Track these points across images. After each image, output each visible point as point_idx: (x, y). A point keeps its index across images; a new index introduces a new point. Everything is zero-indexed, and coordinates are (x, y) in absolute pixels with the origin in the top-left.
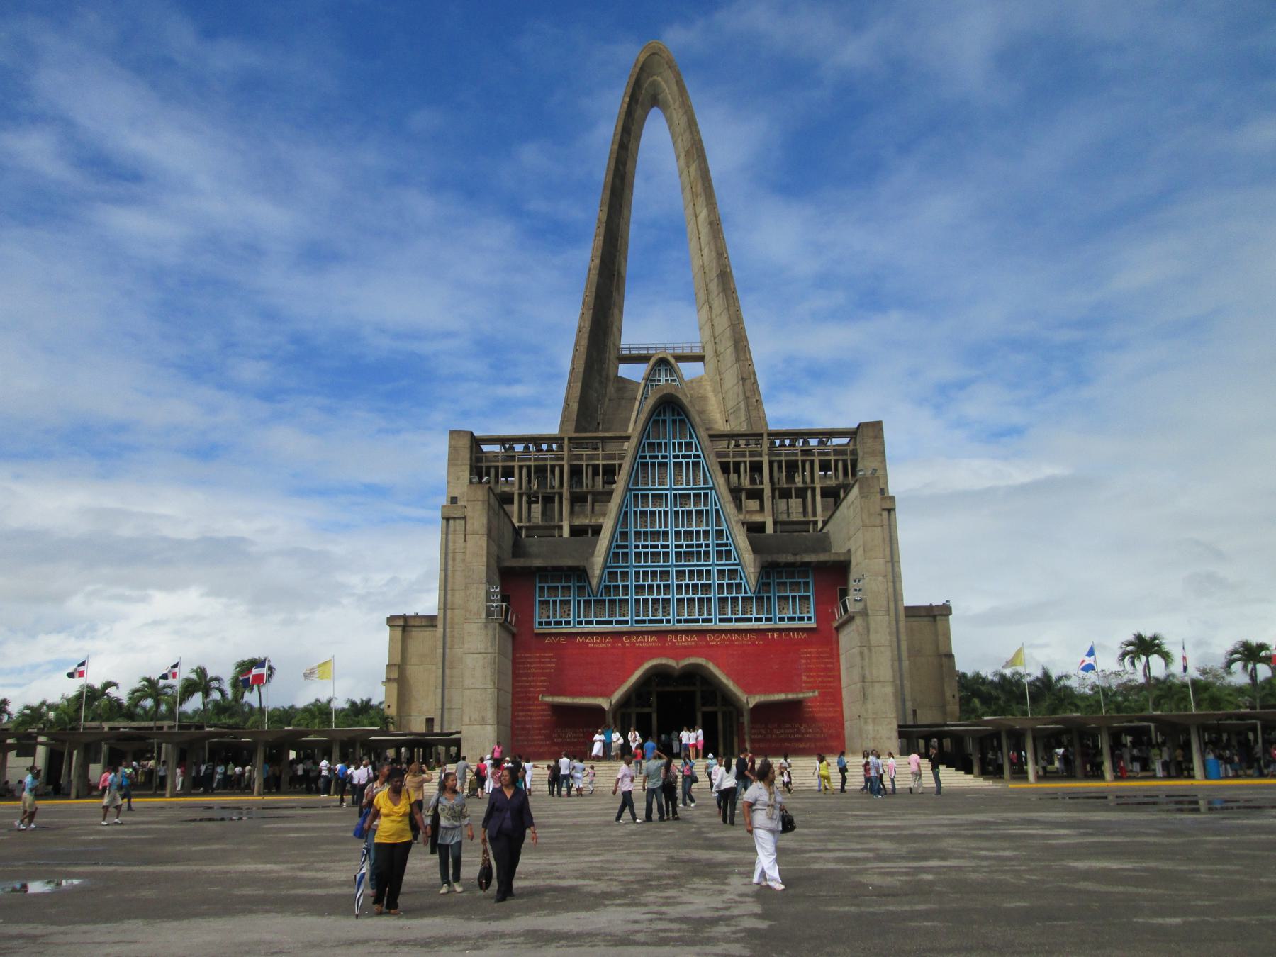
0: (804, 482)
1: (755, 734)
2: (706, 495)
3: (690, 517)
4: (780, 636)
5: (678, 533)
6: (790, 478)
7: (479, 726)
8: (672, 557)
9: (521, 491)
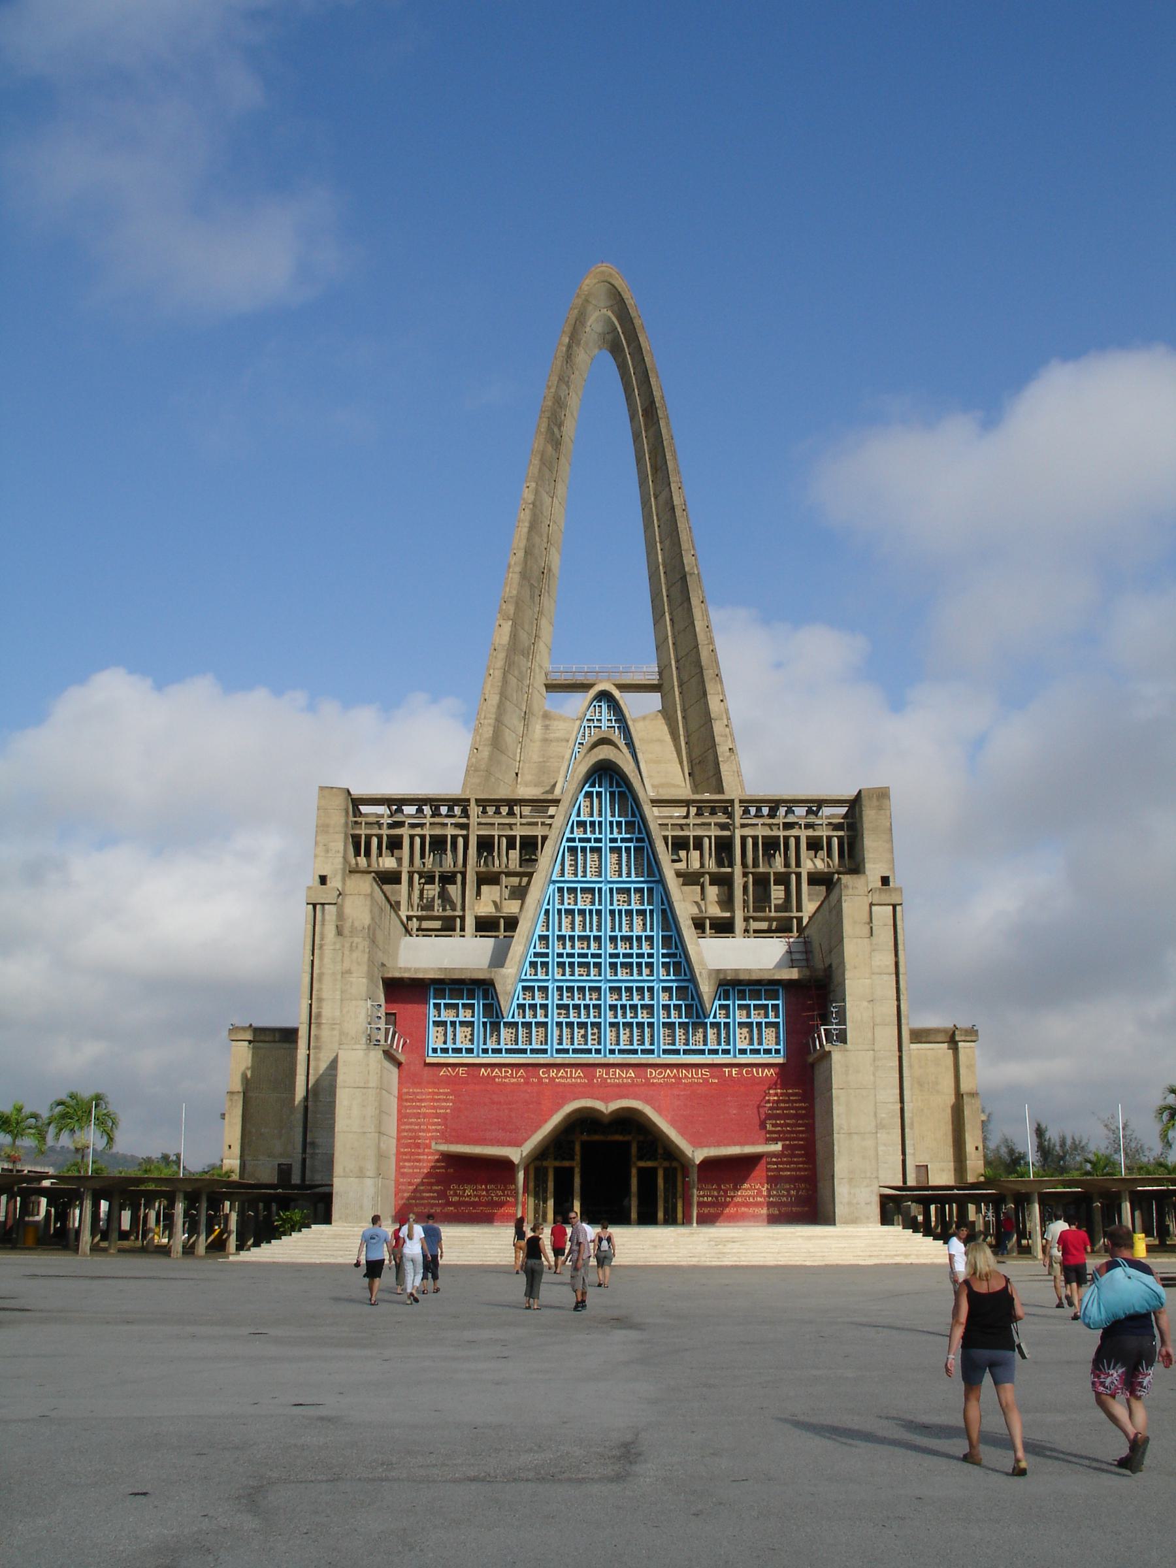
0: (787, 865)
1: (703, 1196)
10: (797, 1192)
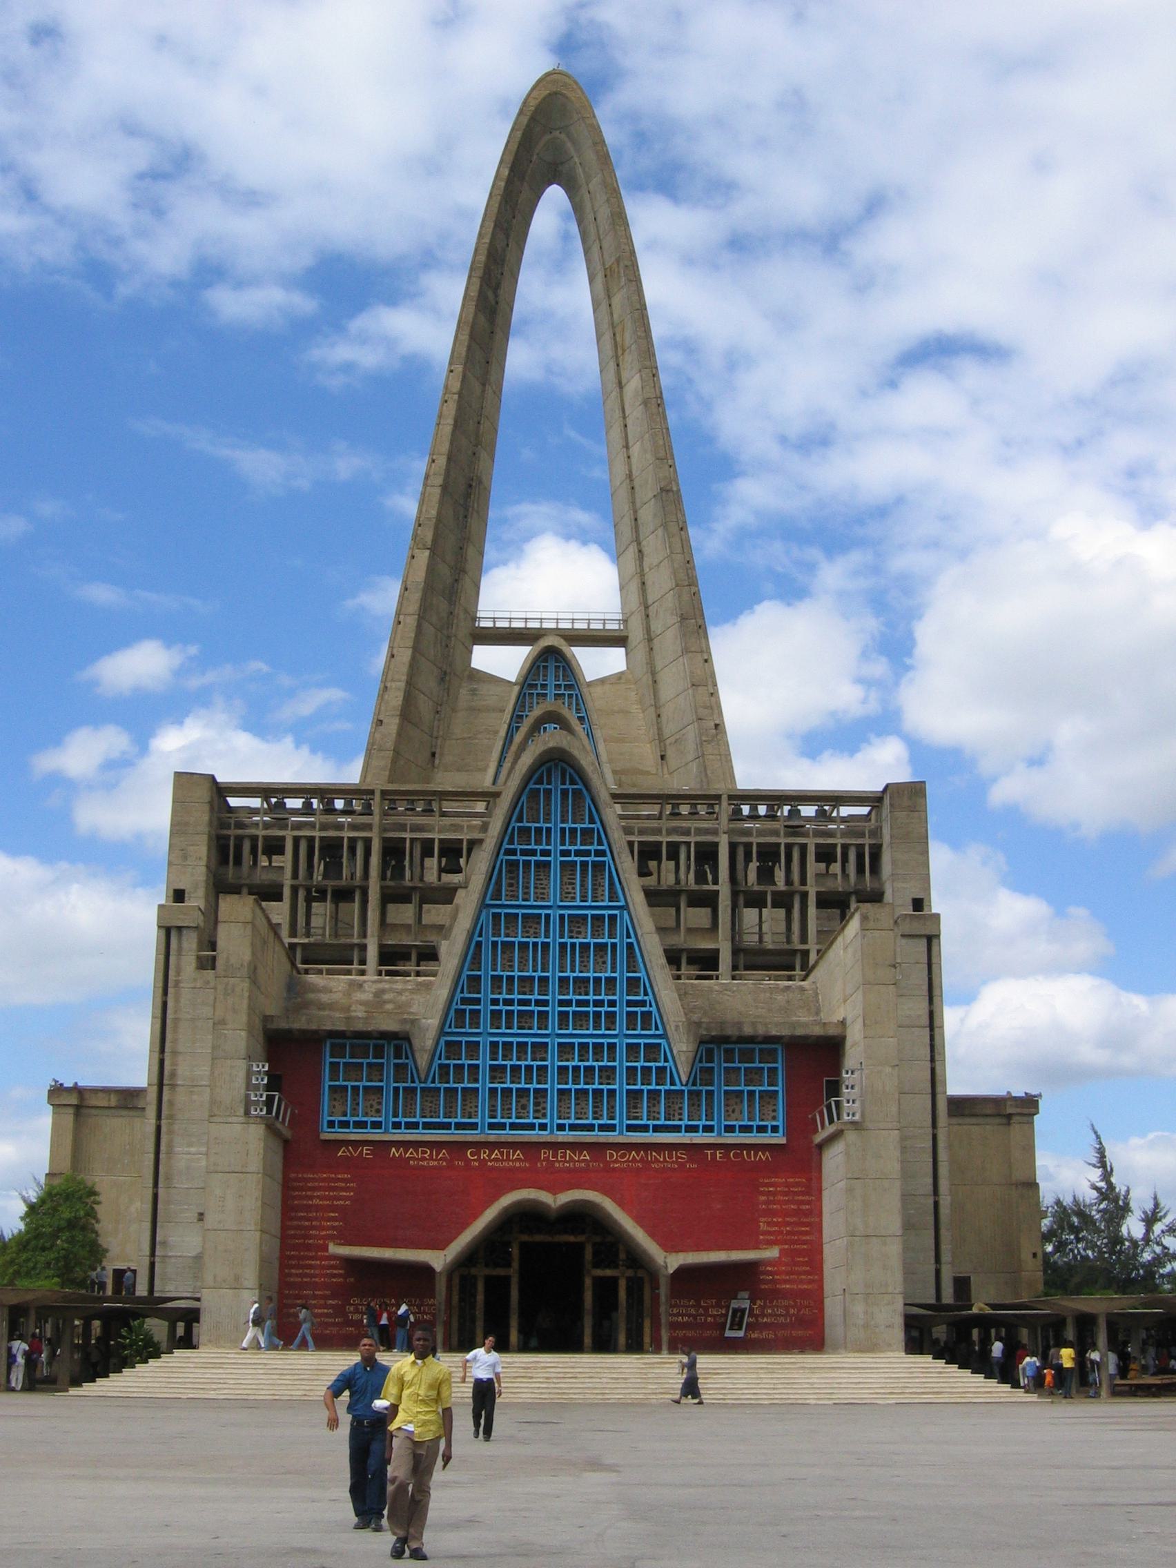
0: (789, 882)
2: (613, 918)
3: (585, 955)
4: (726, 1155)
5: (564, 981)
6: (766, 875)
7: (231, 1292)
8: (553, 1020)
9: (296, 882)
10: (799, 1311)
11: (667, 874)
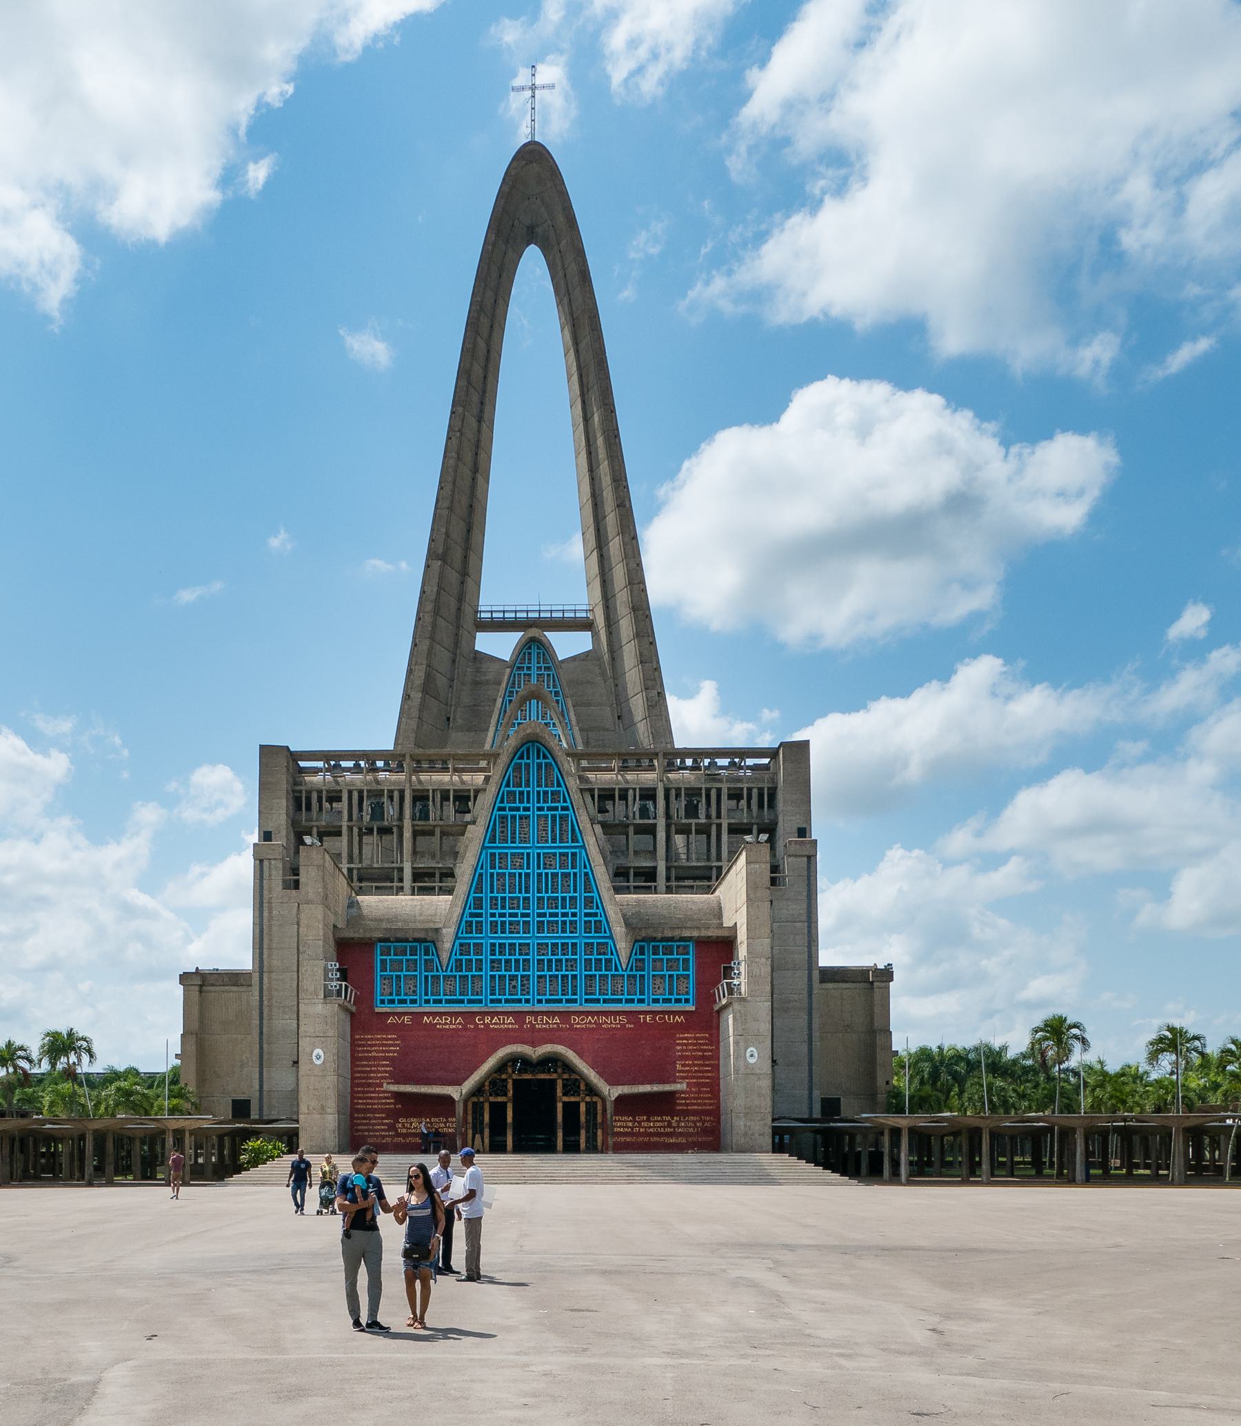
0: (708, 816)
6: (692, 811)
9: (350, 824)
10: (703, 1124)
11: (617, 811)
